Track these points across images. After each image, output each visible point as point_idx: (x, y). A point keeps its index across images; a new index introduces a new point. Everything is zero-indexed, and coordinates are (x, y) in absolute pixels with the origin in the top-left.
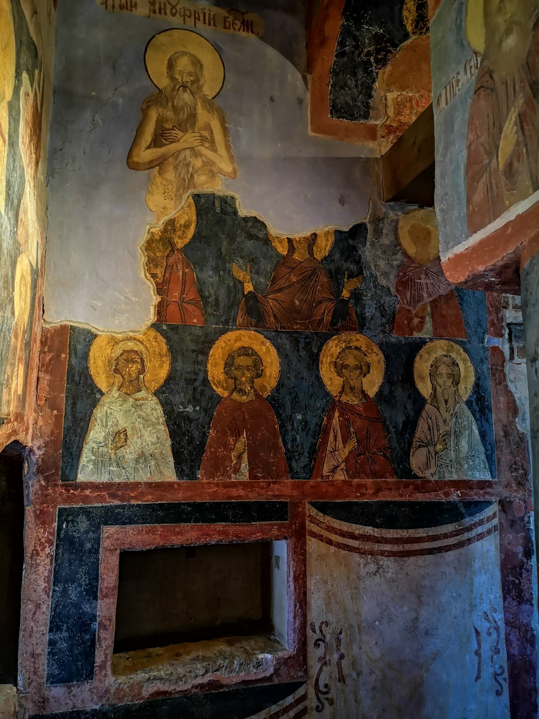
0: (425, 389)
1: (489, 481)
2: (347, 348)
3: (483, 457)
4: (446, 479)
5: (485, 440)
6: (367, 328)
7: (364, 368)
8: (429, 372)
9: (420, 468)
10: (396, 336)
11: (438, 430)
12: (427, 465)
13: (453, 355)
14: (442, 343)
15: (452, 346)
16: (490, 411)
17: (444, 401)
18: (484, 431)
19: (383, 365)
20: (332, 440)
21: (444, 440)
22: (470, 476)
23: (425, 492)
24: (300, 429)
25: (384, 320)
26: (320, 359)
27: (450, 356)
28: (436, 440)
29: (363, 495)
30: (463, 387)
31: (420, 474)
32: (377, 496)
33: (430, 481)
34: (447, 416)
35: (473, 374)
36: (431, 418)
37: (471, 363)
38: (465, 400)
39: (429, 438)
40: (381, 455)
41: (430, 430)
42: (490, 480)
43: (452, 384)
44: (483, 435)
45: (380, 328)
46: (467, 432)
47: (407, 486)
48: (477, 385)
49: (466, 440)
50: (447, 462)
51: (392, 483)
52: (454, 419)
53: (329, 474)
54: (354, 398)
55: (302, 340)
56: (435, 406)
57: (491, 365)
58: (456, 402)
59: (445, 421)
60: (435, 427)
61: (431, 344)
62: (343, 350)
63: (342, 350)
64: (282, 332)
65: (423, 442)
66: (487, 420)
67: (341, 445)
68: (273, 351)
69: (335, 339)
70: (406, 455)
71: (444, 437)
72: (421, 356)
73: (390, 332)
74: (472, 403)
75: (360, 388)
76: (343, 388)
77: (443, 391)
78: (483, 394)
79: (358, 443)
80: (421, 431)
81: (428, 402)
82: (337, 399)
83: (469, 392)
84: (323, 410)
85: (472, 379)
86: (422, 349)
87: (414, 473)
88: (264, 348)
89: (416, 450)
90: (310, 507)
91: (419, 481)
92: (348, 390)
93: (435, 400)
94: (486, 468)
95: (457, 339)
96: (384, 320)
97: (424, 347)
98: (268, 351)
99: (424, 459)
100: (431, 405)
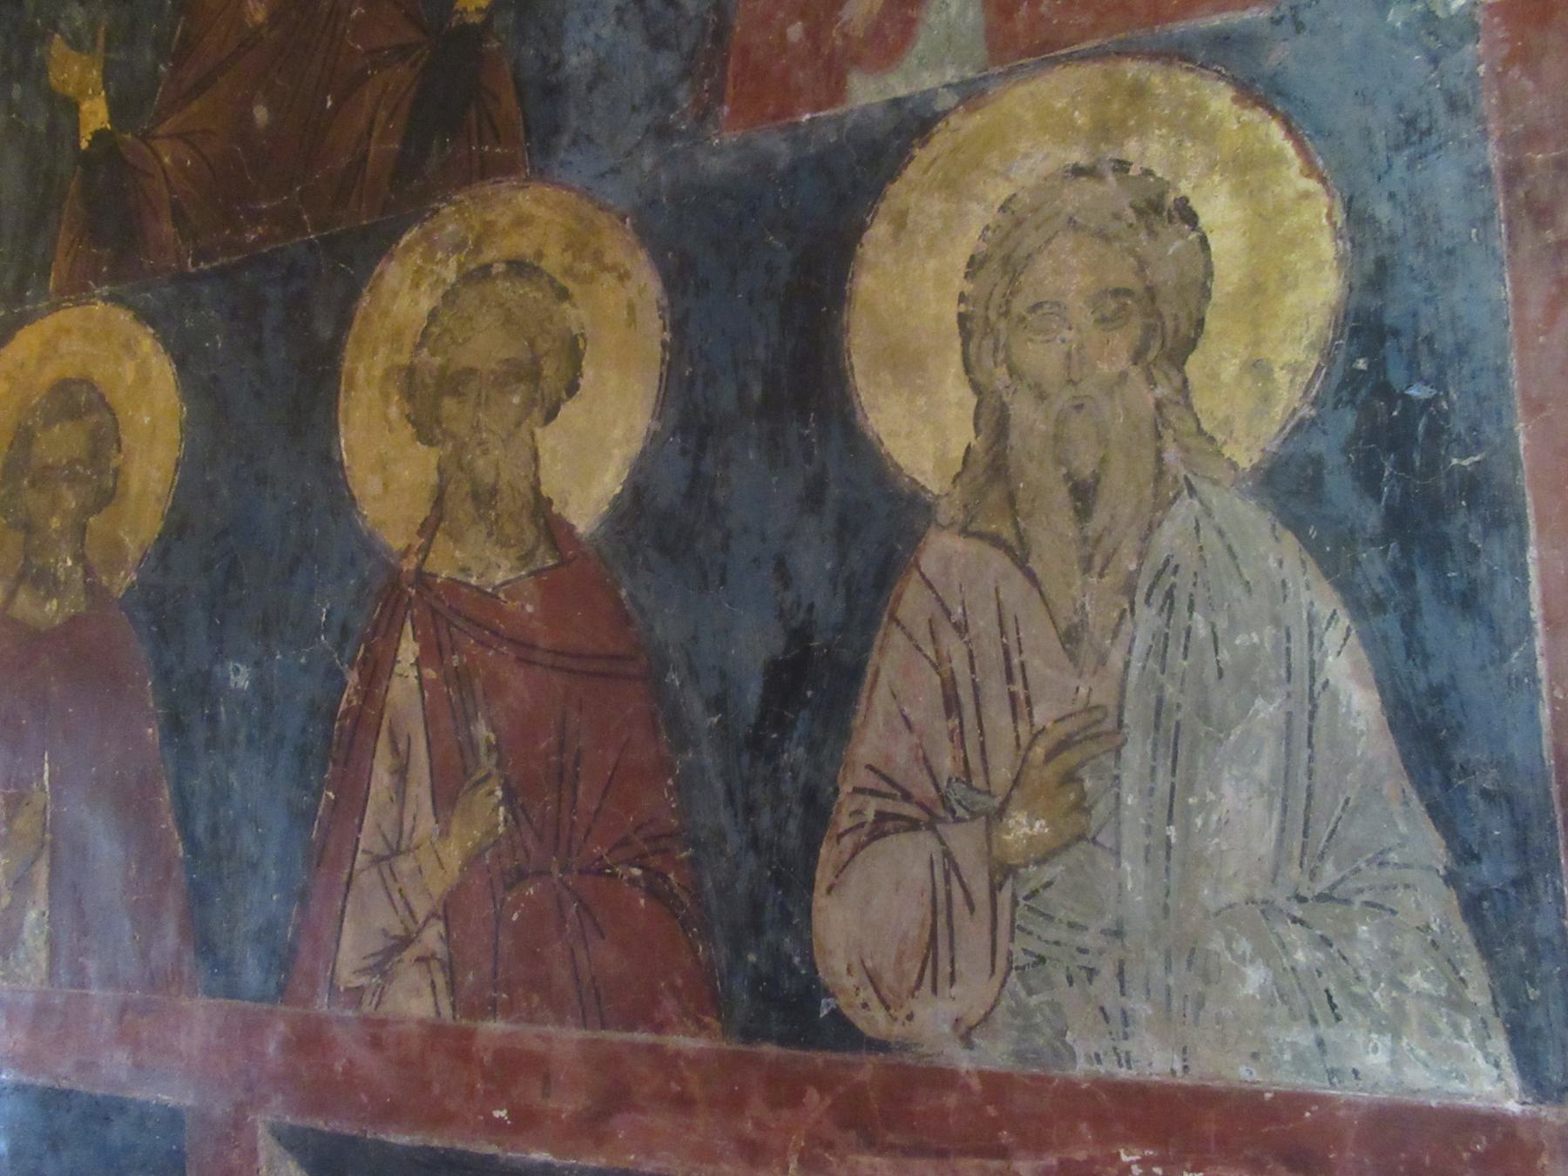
0: (919, 426)
1: (1491, 1122)
2: (466, 277)
3: (1433, 906)
4: (1081, 1069)
5: (1446, 767)
6: (574, 143)
7: (549, 368)
8: (951, 310)
9: (873, 979)
10: (731, 137)
11: (1018, 707)
12: (933, 958)
13: (1149, 151)
14: (1062, 90)
15: (1138, 92)
16: (1503, 517)
17: (1062, 493)
18: (1438, 694)
19: (653, 332)
20: (384, 797)
21: (1070, 778)
22: (1300, 1059)
23: (907, 1152)
24: (241, 737)
25: (667, 64)
26: (346, 365)
27: (1122, 166)
28: (1002, 774)
29: (525, 1121)
30: (1230, 370)
31: (875, 1021)
32: (600, 1141)
33: (945, 1078)
34: (1091, 599)
35: (1327, 247)
36: (961, 628)
37: (1310, 170)
38: (1244, 462)
39: (946, 764)
40: (633, 881)
41: (951, 704)
42: (1513, 1106)
43: (1138, 356)
44: (1427, 733)
45: (643, 119)
46: (1267, 710)
47: (786, 1090)
48: (1365, 329)
49: (1262, 771)
50: (1087, 939)
51: (696, 1061)
52: (1147, 618)
53: (363, 980)
54: (491, 552)
55: (273, 293)
56: (996, 541)
57: (1505, 141)
58: (1163, 490)
59: (1071, 638)
60: (995, 687)
61: (977, 119)
62: (450, 297)
63: (445, 296)
64: (202, 276)
65: (907, 797)
66: (1468, 601)
67: (427, 824)
68: (163, 370)
69: (409, 248)
70: (792, 879)
71: (1071, 757)
72: (900, 222)
73: (701, 119)
74: (1317, 482)
75: (524, 486)
76: (439, 499)
77: (1061, 421)
78: (1418, 392)
79: (511, 810)
80: (894, 717)
81: (942, 518)
82: (409, 565)
83: (1288, 396)
84: (345, 631)
85: (1317, 289)
86: (911, 172)
87: (836, 1014)
88: (129, 371)
89: (858, 848)
90: (278, 1150)
91: (867, 1068)
92: (462, 510)
93: (995, 496)
94: (1457, 1003)
95: (1179, 27)
96: (667, 64)
97: (922, 155)
98: (144, 379)
99: (910, 916)
100: (965, 532)
